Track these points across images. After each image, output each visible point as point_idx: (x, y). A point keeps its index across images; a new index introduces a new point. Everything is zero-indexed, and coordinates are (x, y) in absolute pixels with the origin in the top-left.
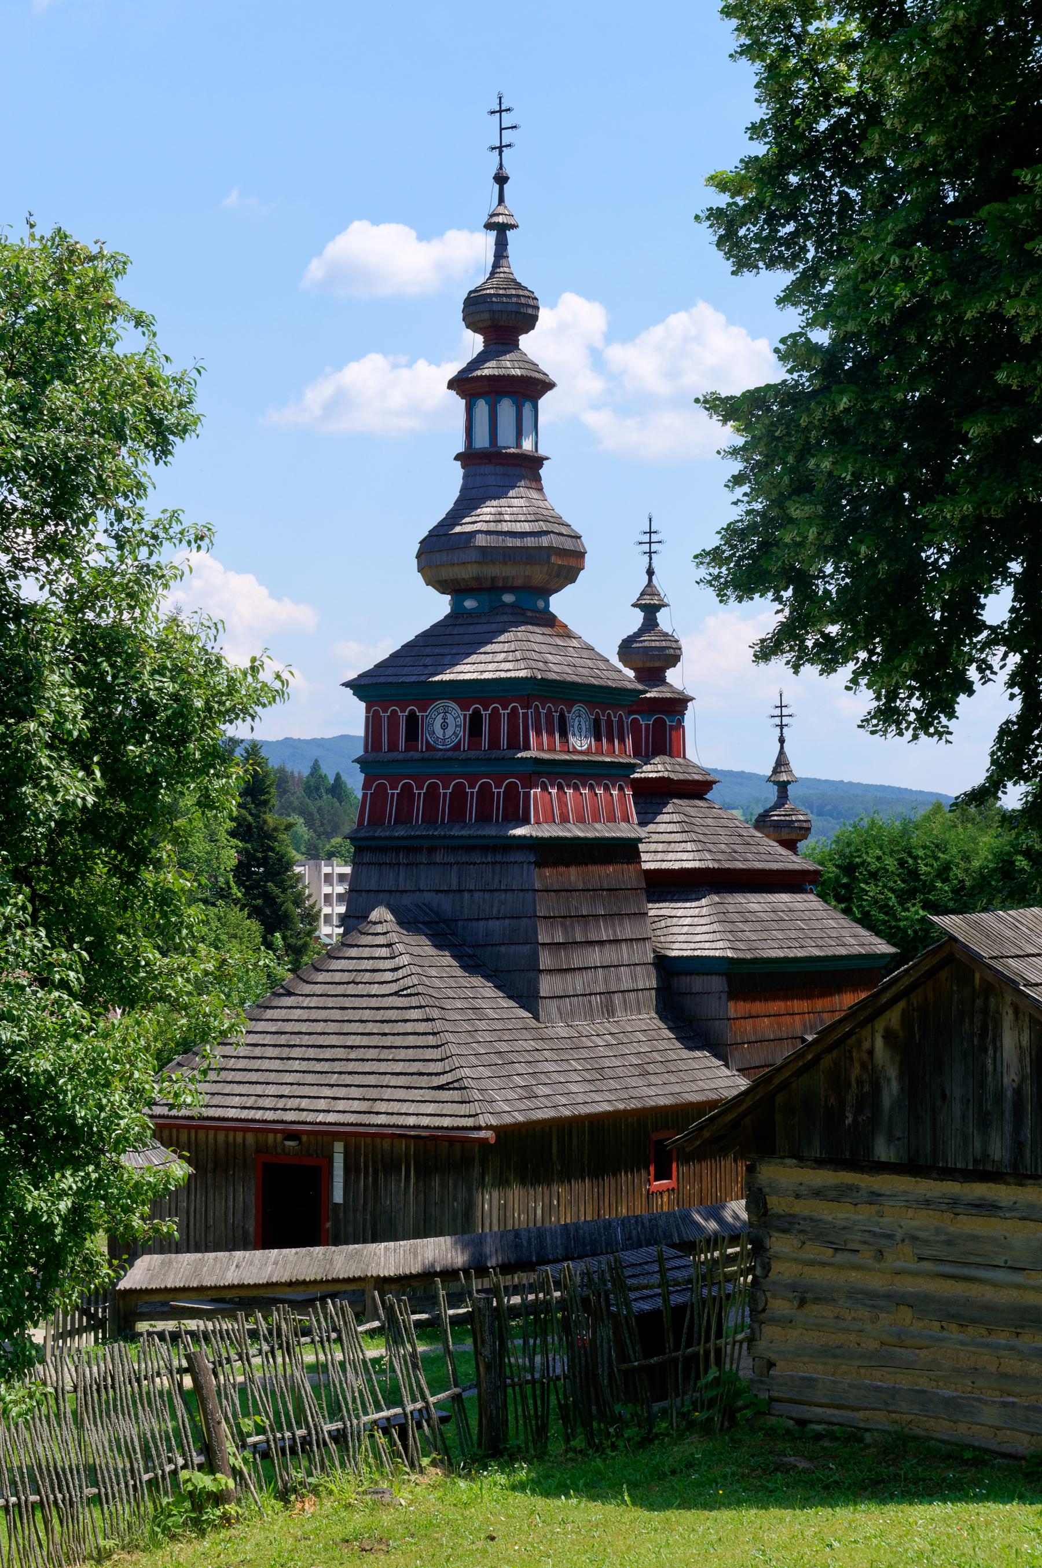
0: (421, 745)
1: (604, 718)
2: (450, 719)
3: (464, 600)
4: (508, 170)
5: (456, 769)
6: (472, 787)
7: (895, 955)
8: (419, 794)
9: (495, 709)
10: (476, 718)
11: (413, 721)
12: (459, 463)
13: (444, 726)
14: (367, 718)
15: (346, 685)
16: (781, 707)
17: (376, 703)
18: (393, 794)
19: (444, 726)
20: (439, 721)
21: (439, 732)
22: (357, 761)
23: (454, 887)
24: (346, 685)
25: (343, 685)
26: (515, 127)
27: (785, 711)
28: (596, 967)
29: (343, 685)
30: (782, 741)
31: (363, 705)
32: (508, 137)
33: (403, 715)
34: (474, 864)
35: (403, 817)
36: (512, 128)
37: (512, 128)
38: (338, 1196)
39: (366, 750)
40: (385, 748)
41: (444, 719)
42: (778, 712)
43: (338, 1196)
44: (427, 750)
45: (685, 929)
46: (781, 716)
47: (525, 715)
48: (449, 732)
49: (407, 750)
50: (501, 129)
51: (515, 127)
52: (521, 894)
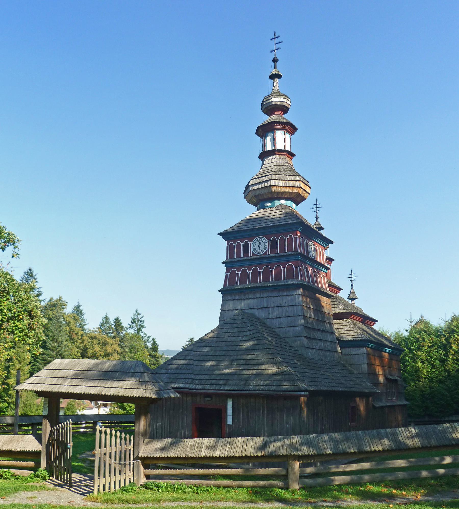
2: (262, 243)
3: (265, 203)
4: (278, 58)
5: (265, 261)
6: (272, 268)
7: (155, 399)
8: (249, 273)
9: (282, 237)
10: (274, 242)
11: (247, 247)
12: (223, 243)
13: (260, 246)
14: (227, 247)
16: (352, 274)
17: (231, 240)
18: (238, 274)
19: (260, 246)
20: (258, 244)
21: (257, 249)
25: (218, 234)
26: (281, 42)
27: (353, 276)
28: (321, 340)
29: (218, 234)
30: (352, 285)
32: (277, 46)
33: (242, 244)
34: (274, 297)
35: (243, 281)
36: (280, 43)
37: (280, 43)
38: (230, 421)
39: (227, 258)
40: (235, 257)
42: (351, 276)
43: (230, 421)
44: (252, 256)
45: (346, 332)
46: (352, 277)
48: (262, 248)
49: (244, 256)
50: (275, 44)
51: (281, 42)
52: (295, 307)
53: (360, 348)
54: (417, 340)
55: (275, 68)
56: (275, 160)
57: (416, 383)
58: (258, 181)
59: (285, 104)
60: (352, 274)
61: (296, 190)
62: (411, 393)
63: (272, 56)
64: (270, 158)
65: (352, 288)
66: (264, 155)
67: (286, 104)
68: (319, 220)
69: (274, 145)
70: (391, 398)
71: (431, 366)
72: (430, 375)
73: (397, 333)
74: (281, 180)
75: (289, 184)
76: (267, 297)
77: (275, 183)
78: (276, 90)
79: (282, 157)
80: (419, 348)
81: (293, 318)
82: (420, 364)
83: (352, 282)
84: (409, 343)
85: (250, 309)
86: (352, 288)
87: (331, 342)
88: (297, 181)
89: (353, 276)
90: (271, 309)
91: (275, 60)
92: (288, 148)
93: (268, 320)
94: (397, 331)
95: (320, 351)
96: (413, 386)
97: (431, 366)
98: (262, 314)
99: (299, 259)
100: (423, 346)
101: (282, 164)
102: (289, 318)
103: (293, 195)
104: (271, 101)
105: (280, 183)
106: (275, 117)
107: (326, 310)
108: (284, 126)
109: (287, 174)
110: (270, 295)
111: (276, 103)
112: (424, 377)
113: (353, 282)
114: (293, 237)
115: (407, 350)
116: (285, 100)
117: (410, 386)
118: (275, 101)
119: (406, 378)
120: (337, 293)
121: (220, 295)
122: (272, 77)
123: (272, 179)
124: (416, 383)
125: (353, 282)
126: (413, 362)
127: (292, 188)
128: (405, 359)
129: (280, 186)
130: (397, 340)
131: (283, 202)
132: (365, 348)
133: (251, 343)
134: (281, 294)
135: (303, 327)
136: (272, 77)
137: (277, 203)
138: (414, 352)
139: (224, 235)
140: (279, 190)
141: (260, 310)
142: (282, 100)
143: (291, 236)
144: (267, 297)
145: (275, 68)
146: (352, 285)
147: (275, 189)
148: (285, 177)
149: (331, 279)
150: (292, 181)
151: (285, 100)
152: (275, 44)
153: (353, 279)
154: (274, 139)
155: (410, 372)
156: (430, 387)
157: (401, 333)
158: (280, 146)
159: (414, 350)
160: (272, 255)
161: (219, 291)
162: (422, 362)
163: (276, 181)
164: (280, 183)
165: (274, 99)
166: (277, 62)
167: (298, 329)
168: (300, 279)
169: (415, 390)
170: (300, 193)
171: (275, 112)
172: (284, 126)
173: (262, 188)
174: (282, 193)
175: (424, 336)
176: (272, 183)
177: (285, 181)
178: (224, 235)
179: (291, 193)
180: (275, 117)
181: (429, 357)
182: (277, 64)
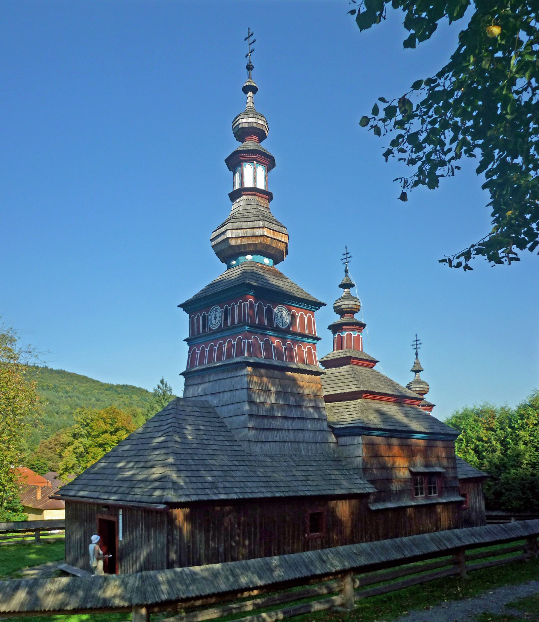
0: (207, 330)
1: (298, 316)
2: (218, 315)
4: (253, 63)
6: (225, 343)
13: (215, 319)
15: (180, 306)
19: (215, 319)
20: (214, 316)
22: (185, 340)
23: (217, 391)
24: (180, 306)
25: (178, 306)
28: (288, 430)
29: (178, 306)
30: (417, 354)
31: (188, 315)
32: (252, 47)
34: (224, 379)
41: (215, 315)
43: (121, 539)
46: (416, 344)
47: (244, 305)
48: (217, 320)
53: (356, 437)
54: (522, 417)
55: (249, 78)
56: (242, 203)
57: (517, 470)
58: (218, 232)
59: (255, 125)
60: (416, 341)
61: (259, 240)
62: (510, 481)
63: (246, 62)
64: (238, 200)
65: (417, 358)
66: (234, 196)
67: (257, 125)
68: (349, 274)
69: (242, 183)
70: (424, 495)
71: (535, 449)
72: (532, 460)
73: (503, 409)
74: (240, 229)
75: (250, 232)
76: (219, 380)
77: (232, 234)
78: (249, 107)
79: (250, 197)
80: (522, 428)
81: (239, 405)
82: (522, 447)
83: (417, 350)
84: (512, 420)
85: (206, 395)
86: (417, 358)
87: (313, 431)
88: (259, 228)
89: (418, 342)
90: (221, 394)
91: (249, 68)
92: (261, 185)
93: (219, 408)
94: (504, 406)
95: (286, 444)
96: (514, 473)
97: (535, 449)
98: (214, 401)
99: (247, 330)
100: (527, 424)
101: (249, 207)
102: (236, 405)
103: (259, 248)
104: (238, 123)
105: (240, 233)
106: (248, 145)
107: (307, 391)
108: (251, 155)
109: (237, 220)
110: (221, 377)
111: (244, 125)
112: (525, 462)
113: (418, 350)
114: (242, 304)
115: (509, 430)
116: (254, 120)
117: (509, 473)
118: (242, 123)
119: (506, 463)
120: (371, 367)
121: (182, 379)
122: (246, 90)
123: (228, 230)
124: (517, 470)
125: (418, 350)
126: (514, 444)
127: (254, 239)
128: (506, 441)
129: (239, 237)
130: (501, 417)
131: (249, 257)
132: (361, 437)
133: (162, 438)
134: (230, 376)
135: (247, 416)
136: (246, 90)
137: (242, 260)
138: (517, 431)
139: (185, 306)
140: (239, 242)
141: (213, 396)
142: (250, 120)
143: (240, 303)
144: (219, 380)
145: (249, 78)
146: (417, 354)
147: (233, 242)
148: (245, 225)
149: (362, 350)
150: (253, 228)
151: (254, 120)
152: (250, 45)
153: (418, 346)
154: (242, 176)
155: (511, 456)
156: (533, 475)
157: (507, 408)
158: (248, 183)
159: (516, 429)
160: (224, 328)
161: (181, 374)
162: (525, 444)
163: (234, 231)
164: (240, 233)
165: (240, 121)
166: (252, 70)
167: (242, 418)
168: (246, 355)
169: (515, 478)
170: (268, 244)
171: (246, 138)
172: (251, 155)
173: (221, 242)
174: (244, 245)
175: (529, 412)
176: (229, 234)
177: (245, 230)
178: (185, 306)
179: (255, 245)
180: (248, 145)
181: (532, 438)
182: (252, 72)
